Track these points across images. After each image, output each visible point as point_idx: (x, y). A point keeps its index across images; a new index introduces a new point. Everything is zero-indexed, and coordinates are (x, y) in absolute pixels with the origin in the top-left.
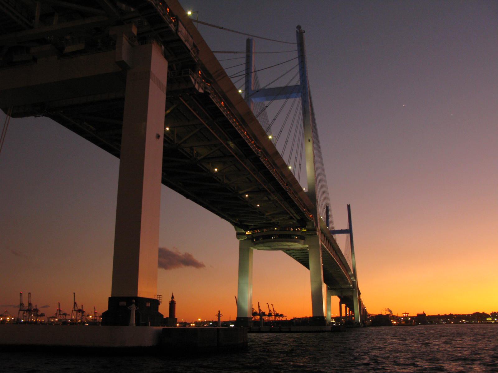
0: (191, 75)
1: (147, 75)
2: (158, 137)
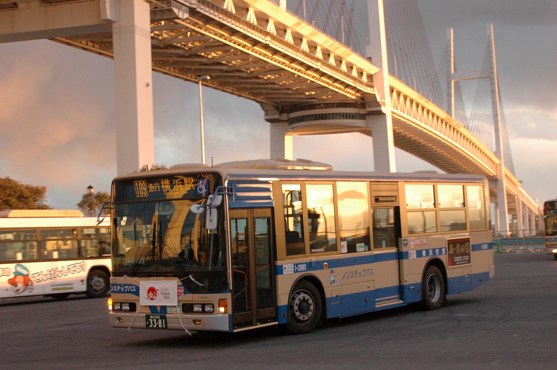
0: (173, 6)
1: (131, 29)
2: (148, 85)
